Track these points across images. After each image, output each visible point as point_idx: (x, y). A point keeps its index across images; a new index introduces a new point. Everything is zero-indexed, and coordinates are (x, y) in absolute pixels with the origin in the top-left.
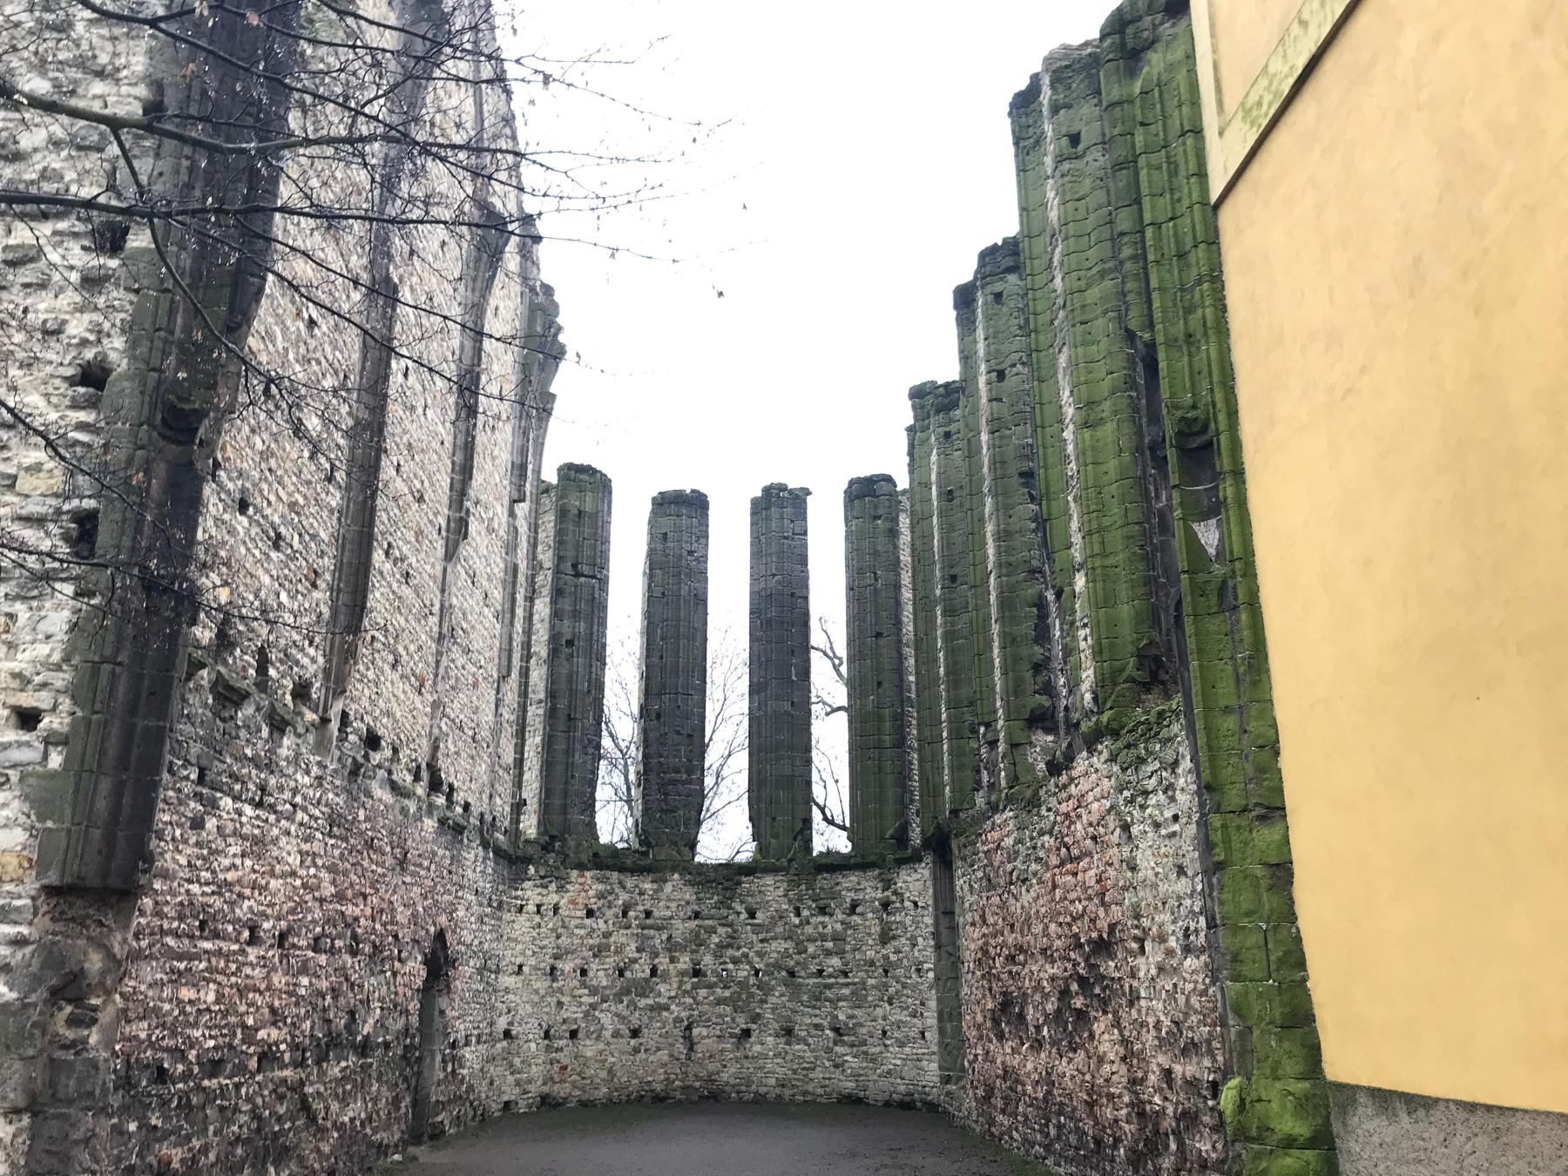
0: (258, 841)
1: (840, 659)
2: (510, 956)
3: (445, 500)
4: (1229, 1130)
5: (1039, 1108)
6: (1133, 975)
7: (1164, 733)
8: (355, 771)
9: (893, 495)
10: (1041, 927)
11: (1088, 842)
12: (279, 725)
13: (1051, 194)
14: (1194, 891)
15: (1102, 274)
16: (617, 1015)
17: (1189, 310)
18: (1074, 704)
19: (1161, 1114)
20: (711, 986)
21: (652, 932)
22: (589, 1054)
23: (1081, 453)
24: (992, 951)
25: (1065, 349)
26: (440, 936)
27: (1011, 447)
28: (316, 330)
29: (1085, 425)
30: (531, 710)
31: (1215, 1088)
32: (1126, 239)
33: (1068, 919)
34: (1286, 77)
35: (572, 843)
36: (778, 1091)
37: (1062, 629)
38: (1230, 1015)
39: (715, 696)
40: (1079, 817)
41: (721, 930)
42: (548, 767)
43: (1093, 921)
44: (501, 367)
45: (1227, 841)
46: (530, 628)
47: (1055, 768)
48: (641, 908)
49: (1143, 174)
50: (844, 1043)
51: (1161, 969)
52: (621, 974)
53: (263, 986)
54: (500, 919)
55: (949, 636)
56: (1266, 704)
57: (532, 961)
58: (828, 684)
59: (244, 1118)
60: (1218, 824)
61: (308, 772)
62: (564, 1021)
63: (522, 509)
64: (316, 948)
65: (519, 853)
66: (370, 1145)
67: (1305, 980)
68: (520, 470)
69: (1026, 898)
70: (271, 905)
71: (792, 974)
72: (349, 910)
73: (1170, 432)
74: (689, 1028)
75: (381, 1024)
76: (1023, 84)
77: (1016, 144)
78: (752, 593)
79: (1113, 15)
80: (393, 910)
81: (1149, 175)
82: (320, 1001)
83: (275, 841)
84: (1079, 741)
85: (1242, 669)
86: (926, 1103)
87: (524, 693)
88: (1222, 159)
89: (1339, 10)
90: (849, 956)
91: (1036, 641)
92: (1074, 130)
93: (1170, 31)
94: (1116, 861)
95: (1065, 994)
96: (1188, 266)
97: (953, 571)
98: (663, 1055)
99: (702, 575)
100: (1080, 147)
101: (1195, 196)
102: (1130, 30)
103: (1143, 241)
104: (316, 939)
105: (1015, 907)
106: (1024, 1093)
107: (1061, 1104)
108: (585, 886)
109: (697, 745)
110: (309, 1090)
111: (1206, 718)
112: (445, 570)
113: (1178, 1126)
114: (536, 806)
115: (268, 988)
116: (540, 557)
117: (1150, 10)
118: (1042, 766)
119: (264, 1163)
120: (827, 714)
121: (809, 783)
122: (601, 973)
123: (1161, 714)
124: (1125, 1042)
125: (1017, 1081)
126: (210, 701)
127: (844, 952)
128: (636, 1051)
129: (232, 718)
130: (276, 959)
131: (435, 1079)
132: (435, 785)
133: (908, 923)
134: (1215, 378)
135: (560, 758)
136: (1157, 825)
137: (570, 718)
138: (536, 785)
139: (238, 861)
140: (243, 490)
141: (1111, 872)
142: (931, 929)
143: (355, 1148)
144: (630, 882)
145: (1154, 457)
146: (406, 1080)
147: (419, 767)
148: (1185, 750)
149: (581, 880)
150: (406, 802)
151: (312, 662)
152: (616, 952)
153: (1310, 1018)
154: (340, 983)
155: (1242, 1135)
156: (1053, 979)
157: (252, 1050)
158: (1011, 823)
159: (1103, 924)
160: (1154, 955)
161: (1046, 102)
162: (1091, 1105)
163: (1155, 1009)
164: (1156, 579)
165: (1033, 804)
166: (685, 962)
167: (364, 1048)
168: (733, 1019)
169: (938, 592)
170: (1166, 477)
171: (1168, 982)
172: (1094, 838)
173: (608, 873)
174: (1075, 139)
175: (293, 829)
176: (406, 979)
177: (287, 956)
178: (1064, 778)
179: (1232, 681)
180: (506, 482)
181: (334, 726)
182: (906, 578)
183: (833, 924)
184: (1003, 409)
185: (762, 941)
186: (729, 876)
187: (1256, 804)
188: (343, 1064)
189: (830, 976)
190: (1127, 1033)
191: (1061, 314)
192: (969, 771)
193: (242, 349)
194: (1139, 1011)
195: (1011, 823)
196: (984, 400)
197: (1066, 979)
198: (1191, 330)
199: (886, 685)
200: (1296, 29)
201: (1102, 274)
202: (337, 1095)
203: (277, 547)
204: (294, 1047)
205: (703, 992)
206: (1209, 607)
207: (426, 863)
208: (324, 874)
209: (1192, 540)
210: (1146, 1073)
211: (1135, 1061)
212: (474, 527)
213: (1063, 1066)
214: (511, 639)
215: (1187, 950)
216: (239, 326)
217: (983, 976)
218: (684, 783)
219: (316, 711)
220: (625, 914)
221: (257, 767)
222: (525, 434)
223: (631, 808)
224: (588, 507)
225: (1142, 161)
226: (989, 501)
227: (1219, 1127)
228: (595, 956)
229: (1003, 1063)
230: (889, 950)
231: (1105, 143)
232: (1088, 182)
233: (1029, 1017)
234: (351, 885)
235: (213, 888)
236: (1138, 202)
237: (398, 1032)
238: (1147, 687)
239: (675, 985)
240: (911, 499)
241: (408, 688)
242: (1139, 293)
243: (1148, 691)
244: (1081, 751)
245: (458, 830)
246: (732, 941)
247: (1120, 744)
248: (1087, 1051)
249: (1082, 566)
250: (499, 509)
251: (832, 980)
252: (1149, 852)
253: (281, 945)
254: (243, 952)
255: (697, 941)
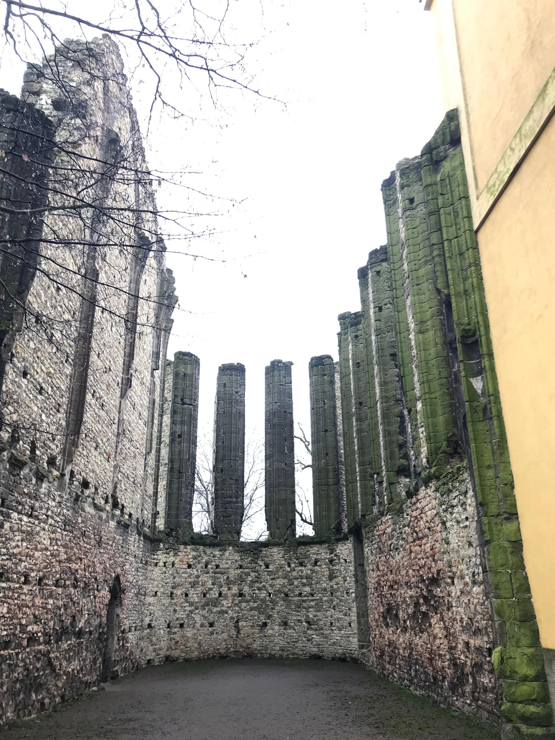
0: (30, 533)
1: (308, 442)
2: (151, 588)
3: (121, 370)
4: (496, 672)
5: (406, 661)
6: (449, 595)
7: (460, 478)
8: (77, 499)
9: (332, 365)
10: (405, 571)
11: (426, 530)
12: (40, 477)
13: (401, 226)
14: (476, 554)
15: (426, 262)
16: (203, 616)
17: (465, 279)
18: (418, 464)
19: (465, 664)
20: (248, 601)
21: (219, 575)
22: (189, 635)
23: (418, 345)
24: (382, 583)
25: (409, 297)
26: (117, 578)
27: (386, 342)
28: (60, 292)
29: (420, 332)
30: (161, 469)
31: (490, 651)
32: (435, 247)
33: (418, 568)
34: (506, 173)
35: (180, 532)
36: (280, 652)
37: (411, 428)
38: (495, 615)
39: (249, 461)
40: (422, 518)
41: (253, 574)
42: (169, 496)
43: (430, 569)
44: (146, 312)
45: (490, 530)
46: (161, 430)
47: (410, 495)
48: (214, 563)
49: (442, 217)
50: (312, 629)
51: (462, 592)
52: (205, 596)
53: (30, 604)
54: (146, 569)
55: (359, 431)
56: (507, 463)
57: (162, 590)
58: (302, 454)
59: (20, 670)
60: (486, 522)
61: (54, 500)
62: (177, 619)
63: (157, 373)
64: (57, 585)
65: (156, 537)
66: (82, 682)
67: (530, 598)
68: (156, 355)
69: (398, 558)
70: (35, 564)
71: (287, 595)
72: (74, 566)
73: (458, 336)
74: (237, 622)
75: (88, 622)
76: (387, 176)
77: (385, 203)
78: (266, 411)
79: (426, 145)
80: (95, 566)
81: (445, 218)
82: (58, 611)
83: (38, 533)
84: (421, 482)
85: (495, 447)
86: (352, 659)
87: (158, 460)
88: (478, 210)
89: (528, 143)
90: (314, 586)
91: (400, 434)
92: (411, 197)
93: (453, 153)
94: (439, 539)
95: (417, 605)
96: (464, 259)
97: (360, 401)
98: (225, 636)
99: (242, 403)
100: (414, 204)
101: (467, 227)
102: (434, 152)
103: (443, 248)
104: (57, 581)
105: (393, 562)
106: (399, 654)
107: (417, 659)
108: (187, 553)
109: (240, 484)
110: (52, 655)
111: (479, 471)
112: (121, 402)
113: (473, 670)
114: (164, 514)
115: (33, 605)
116: (166, 395)
117: (443, 143)
118: (404, 493)
119: (30, 692)
120: (303, 469)
121: (294, 502)
122: (195, 595)
123: (459, 469)
124: (446, 628)
125: (395, 648)
126: (8, 467)
127: (312, 584)
128: (212, 633)
129: (18, 474)
130: (37, 591)
131: (114, 649)
132: (115, 505)
133: (342, 570)
134: (479, 310)
135: (175, 491)
136: (458, 522)
137: (180, 473)
138: (164, 504)
139: (20, 544)
140: (25, 367)
141: (437, 545)
142: (353, 573)
143: (74, 684)
144: (208, 551)
145: (451, 348)
146: (100, 650)
147: (107, 496)
148: (469, 486)
149: (185, 550)
150: (101, 513)
151: (55, 448)
152: (202, 585)
153: (533, 617)
154: (68, 602)
155: (502, 675)
156: (411, 597)
157: (24, 636)
158: (390, 521)
159: (434, 570)
160: (459, 585)
161: (398, 184)
162: (431, 660)
163: (460, 612)
164: (455, 404)
165: (400, 512)
166: (235, 589)
167: (79, 634)
168: (259, 618)
169: (354, 410)
170: (457, 357)
171: (466, 599)
172: (429, 528)
173: (198, 547)
174: (412, 201)
175: (47, 527)
176: (101, 599)
177: (42, 589)
178: (414, 500)
179: (490, 454)
180: (150, 361)
181: (67, 477)
182: (338, 404)
183: (306, 571)
184: (382, 325)
185: (272, 579)
186: (256, 548)
187: (504, 512)
188: (69, 642)
189: (305, 596)
190: (447, 624)
191: (407, 281)
192: (369, 495)
193: (24, 303)
194: (452, 613)
195: (390, 521)
196: (373, 321)
197: (417, 597)
198: (467, 288)
199: (330, 455)
200: (509, 152)
201: (426, 262)
202: (65, 658)
203: (40, 393)
204: (45, 634)
205: (244, 604)
206: (479, 418)
207: (111, 543)
208: (61, 549)
209: (470, 387)
210: (457, 644)
211: (451, 638)
212: (134, 382)
213: (417, 640)
214: (152, 434)
215: (474, 583)
216: (24, 291)
217: (378, 596)
218: (234, 503)
219: (58, 471)
220: (206, 566)
221: (30, 498)
222: (159, 337)
223: (209, 516)
224: (189, 372)
225: (442, 211)
226: (376, 367)
227: (492, 671)
228: (192, 587)
229: (388, 638)
230: (333, 583)
231: (426, 202)
232: (418, 220)
233: (400, 616)
234: (75, 554)
235: (7, 557)
236: (440, 229)
237: (97, 625)
238: (452, 455)
239: (231, 601)
240: (340, 366)
241: (102, 459)
242: (442, 272)
243: (452, 458)
244: (422, 486)
245: (126, 526)
246: (258, 579)
247: (440, 483)
248: (428, 633)
249: (420, 398)
250: (146, 373)
251: (306, 598)
252: (455, 535)
253: (39, 584)
254: (21, 588)
255: (241, 580)
